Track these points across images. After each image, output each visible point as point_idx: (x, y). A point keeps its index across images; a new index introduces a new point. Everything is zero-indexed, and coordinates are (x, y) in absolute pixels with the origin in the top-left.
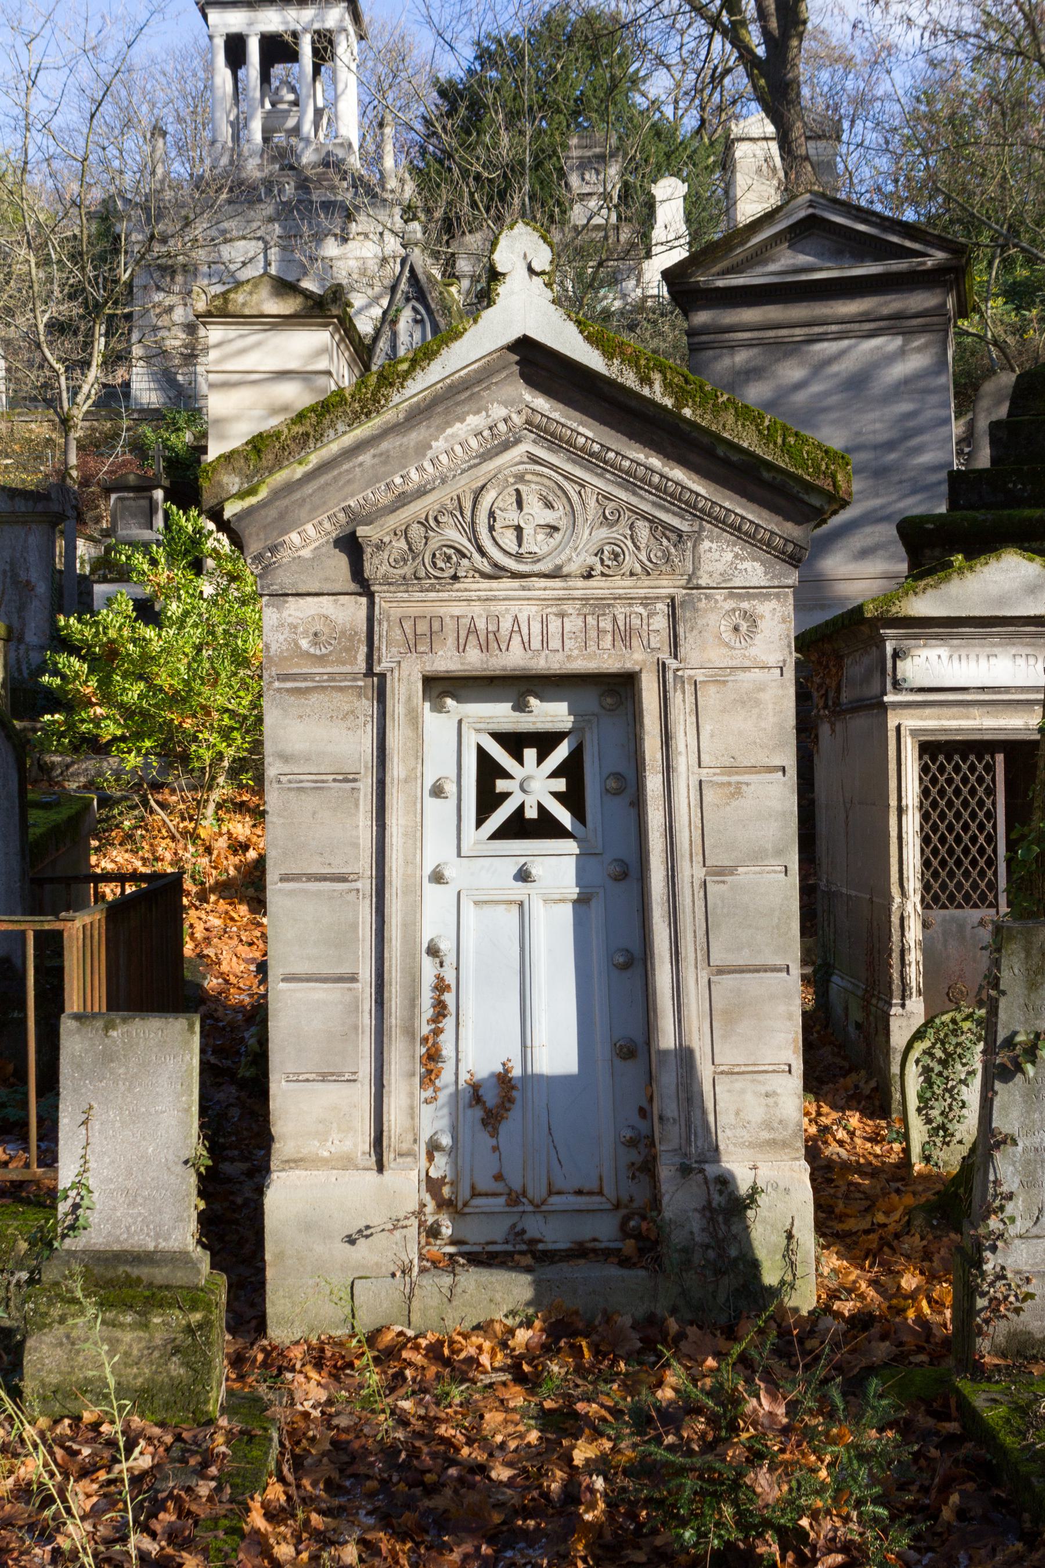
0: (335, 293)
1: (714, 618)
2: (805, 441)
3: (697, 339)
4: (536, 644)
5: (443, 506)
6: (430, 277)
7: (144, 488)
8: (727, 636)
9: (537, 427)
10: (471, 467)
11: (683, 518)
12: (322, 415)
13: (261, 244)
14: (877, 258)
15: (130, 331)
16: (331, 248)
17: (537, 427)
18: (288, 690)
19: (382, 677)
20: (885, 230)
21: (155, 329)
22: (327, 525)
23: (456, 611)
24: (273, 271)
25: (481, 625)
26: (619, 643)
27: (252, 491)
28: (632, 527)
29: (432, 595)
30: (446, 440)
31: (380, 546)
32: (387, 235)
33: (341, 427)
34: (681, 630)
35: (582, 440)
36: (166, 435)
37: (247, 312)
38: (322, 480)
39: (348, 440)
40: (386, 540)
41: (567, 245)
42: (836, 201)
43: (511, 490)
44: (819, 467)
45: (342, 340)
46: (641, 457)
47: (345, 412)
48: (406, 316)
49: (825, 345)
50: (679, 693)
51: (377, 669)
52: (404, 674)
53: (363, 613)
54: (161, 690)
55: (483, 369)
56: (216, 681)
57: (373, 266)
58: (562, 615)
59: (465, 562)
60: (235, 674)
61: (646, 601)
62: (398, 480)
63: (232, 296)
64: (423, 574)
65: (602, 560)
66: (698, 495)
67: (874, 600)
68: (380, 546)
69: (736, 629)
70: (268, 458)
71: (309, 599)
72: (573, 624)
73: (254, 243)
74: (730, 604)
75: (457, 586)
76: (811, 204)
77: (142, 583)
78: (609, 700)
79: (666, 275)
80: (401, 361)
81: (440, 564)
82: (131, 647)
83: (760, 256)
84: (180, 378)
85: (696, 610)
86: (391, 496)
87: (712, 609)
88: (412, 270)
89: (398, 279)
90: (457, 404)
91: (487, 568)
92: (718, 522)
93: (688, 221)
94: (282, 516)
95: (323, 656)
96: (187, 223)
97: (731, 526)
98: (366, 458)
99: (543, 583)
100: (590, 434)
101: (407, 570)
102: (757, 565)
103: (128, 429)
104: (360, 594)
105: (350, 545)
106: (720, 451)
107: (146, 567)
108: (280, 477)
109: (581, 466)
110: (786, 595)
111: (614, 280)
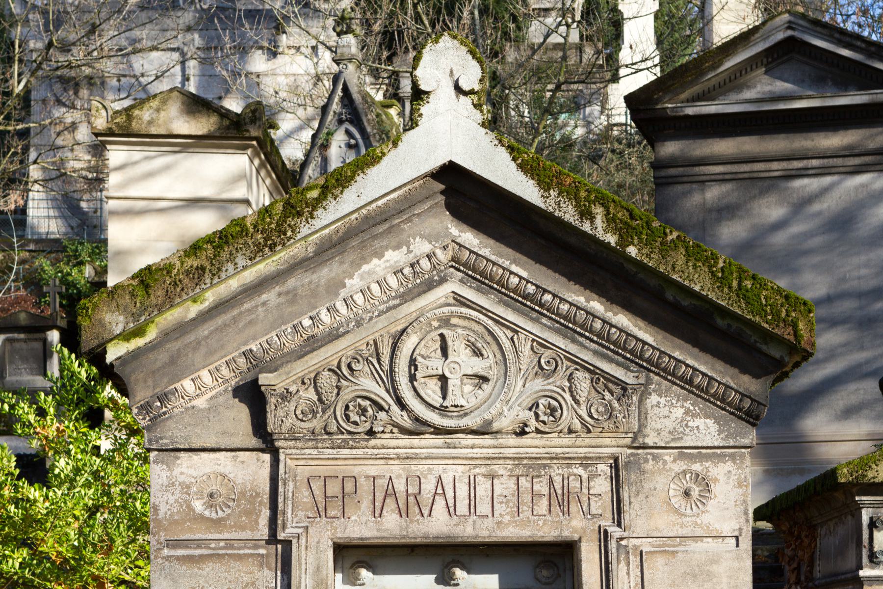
0: (254, 112)
1: (662, 479)
2: (763, 286)
3: (664, 173)
4: (462, 508)
5: (358, 352)
6: (365, 96)
7: (37, 328)
8: (677, 501)
9: (465, 265)
10: (390, 309)
11: (627, 368)
12: (220, 247)
13: (176, 56)
14: (863, 87)
15: (26, 150)
16: (258, 62)
17: (465, 265)
18: (178, 558)
19: (287, 544)
20: (871, 55)
21: (55, 148)
22: (225, 371)
23: (373, 471)
24: (192, 88)
25: (400, 486)
26: (556, 509)
27: (139, 332)
28: (570, 378)
29: (345, 452)
30: (362, 278)
31: (286, 396)
32: (321, 49)
33: (241, 261)
34: (625, 495)
35: (514, 280)
36: (67, 269)
37: (154, 131)
38: (220, 321)
39: (250, 275)
40: (293, 389)
41: (520, 65)
42: (817, 23)
43: (435, 335)
44: (778, 314)
45: (262, 165)
46: (581, 300)
47: (246, 244)
48: (339, 140)
49: (805, 181)
50: (623, 565)
51: (281, 536)
52: (313, 541)
53: (265, 472)
54: (49, 559)
55: (405, 197)
56: (110, 548)
57: (306, 85)
58: (492, 477)
59: (382, 415)
60: (134, 541)
61: (586, 462)
62: (307, 322)
63: (136, 112)
64: (333, 428)
65: (537, 415)
66: (645, 343)
67: (849, 463)
68: (286, 396)
69: (687, 494)
70: (158, 294)
71: (204, 455)
72: (505, 486)
73: (168, 54)
74: (680, 466)
75: (373, 442)
76: (790, 26)
77: (28, 436)
78: (545, 573)
79: (631, 100)
80: (310, 188)
81: (354, 417)
82: (12, 508)
83: (734, 81)
84: (84, 205)
85: (643, 472)
86: (298, 340)
87: (660, 471)
88: (346, 89)
89: (330, 98)
90: (374, 237)
91: (407, 423)
92: (669, 374)
93: (659, 43)
94: (173, 361)
95: (220, 520)
96: (93, 29)
97: (681, 378)
98: (270, 296)
99: (470, 440)
100: (524, 274)
101: (316, 424)
102: (710, 422)
103: (22, 262)
104: (263, 451)
105: (252, 395)
106: (670, 295)
107: (32, 418)
108: (172, 316)
109: (515, 309)
110: (742, 456)
111: (575, 106)
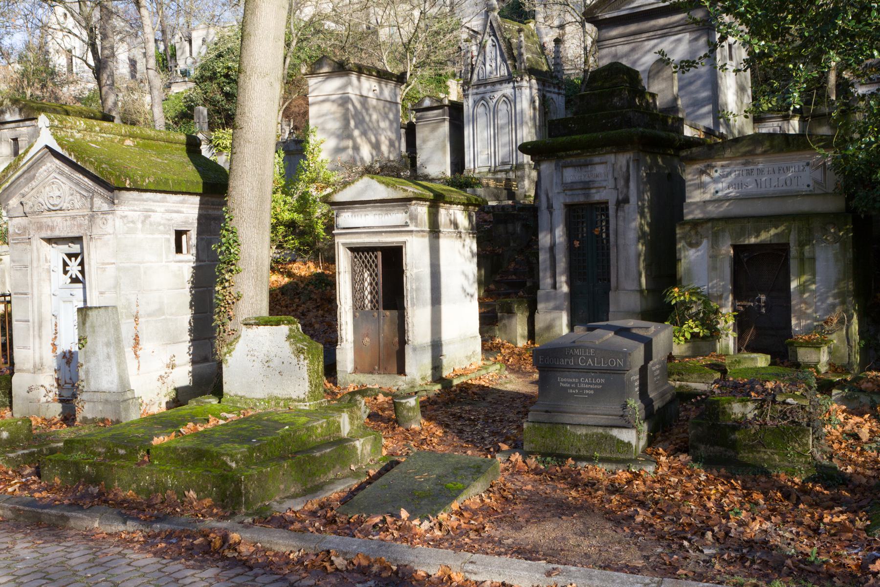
98: (22, 179)
